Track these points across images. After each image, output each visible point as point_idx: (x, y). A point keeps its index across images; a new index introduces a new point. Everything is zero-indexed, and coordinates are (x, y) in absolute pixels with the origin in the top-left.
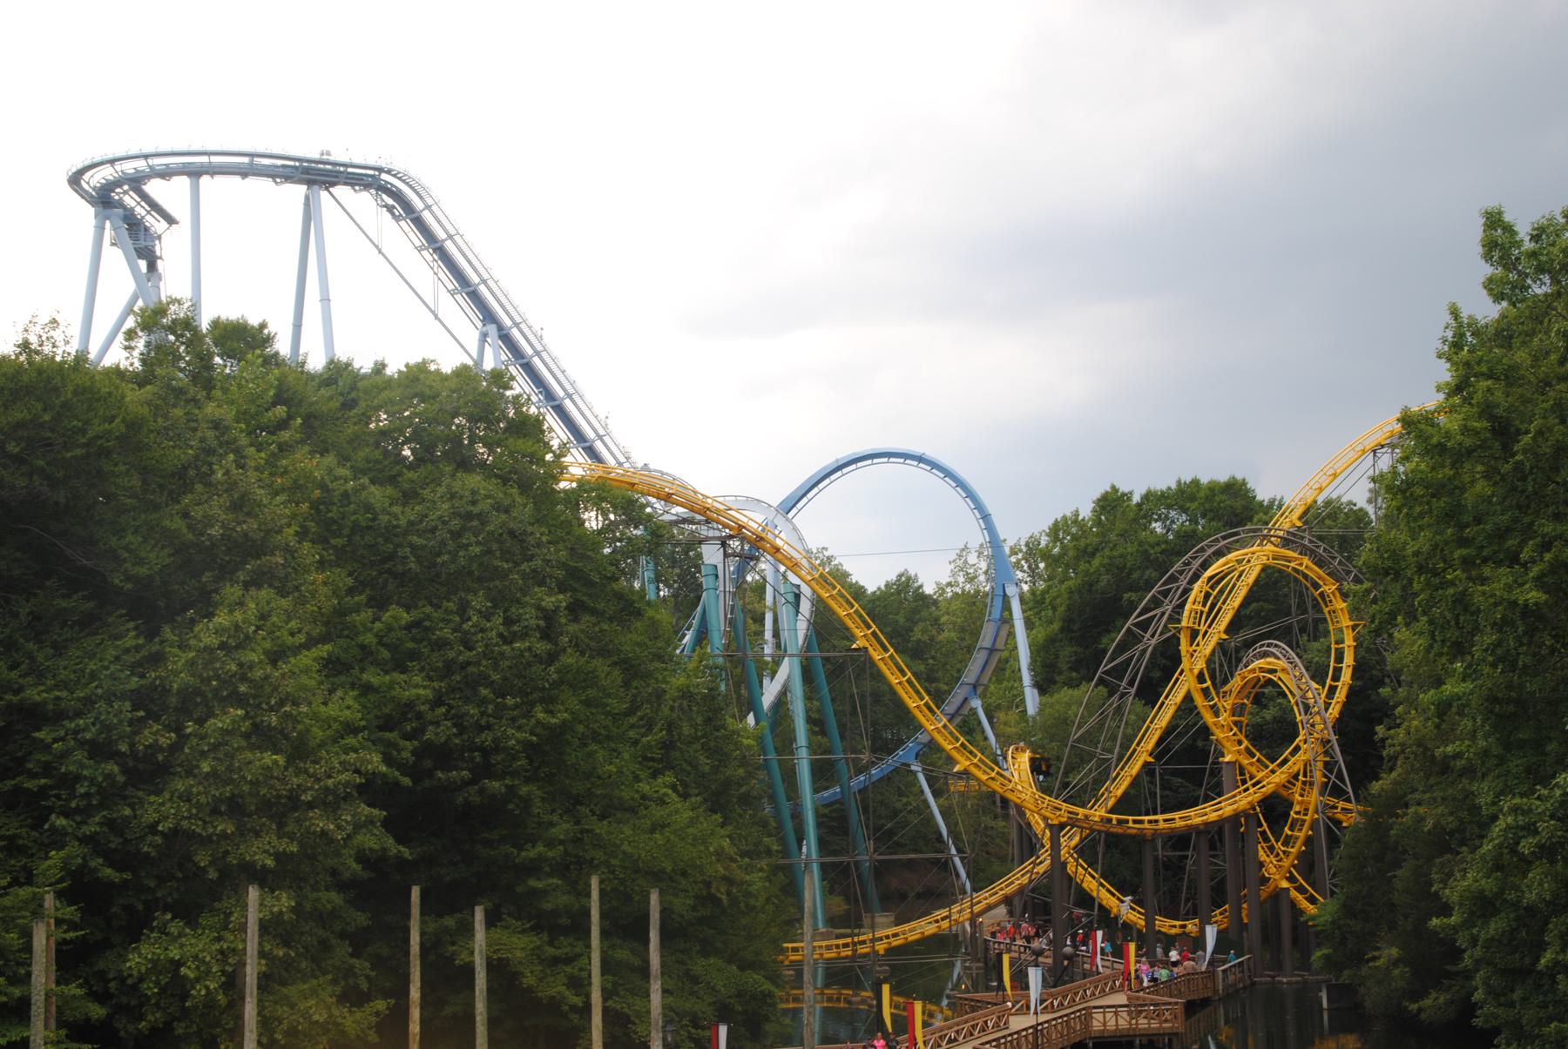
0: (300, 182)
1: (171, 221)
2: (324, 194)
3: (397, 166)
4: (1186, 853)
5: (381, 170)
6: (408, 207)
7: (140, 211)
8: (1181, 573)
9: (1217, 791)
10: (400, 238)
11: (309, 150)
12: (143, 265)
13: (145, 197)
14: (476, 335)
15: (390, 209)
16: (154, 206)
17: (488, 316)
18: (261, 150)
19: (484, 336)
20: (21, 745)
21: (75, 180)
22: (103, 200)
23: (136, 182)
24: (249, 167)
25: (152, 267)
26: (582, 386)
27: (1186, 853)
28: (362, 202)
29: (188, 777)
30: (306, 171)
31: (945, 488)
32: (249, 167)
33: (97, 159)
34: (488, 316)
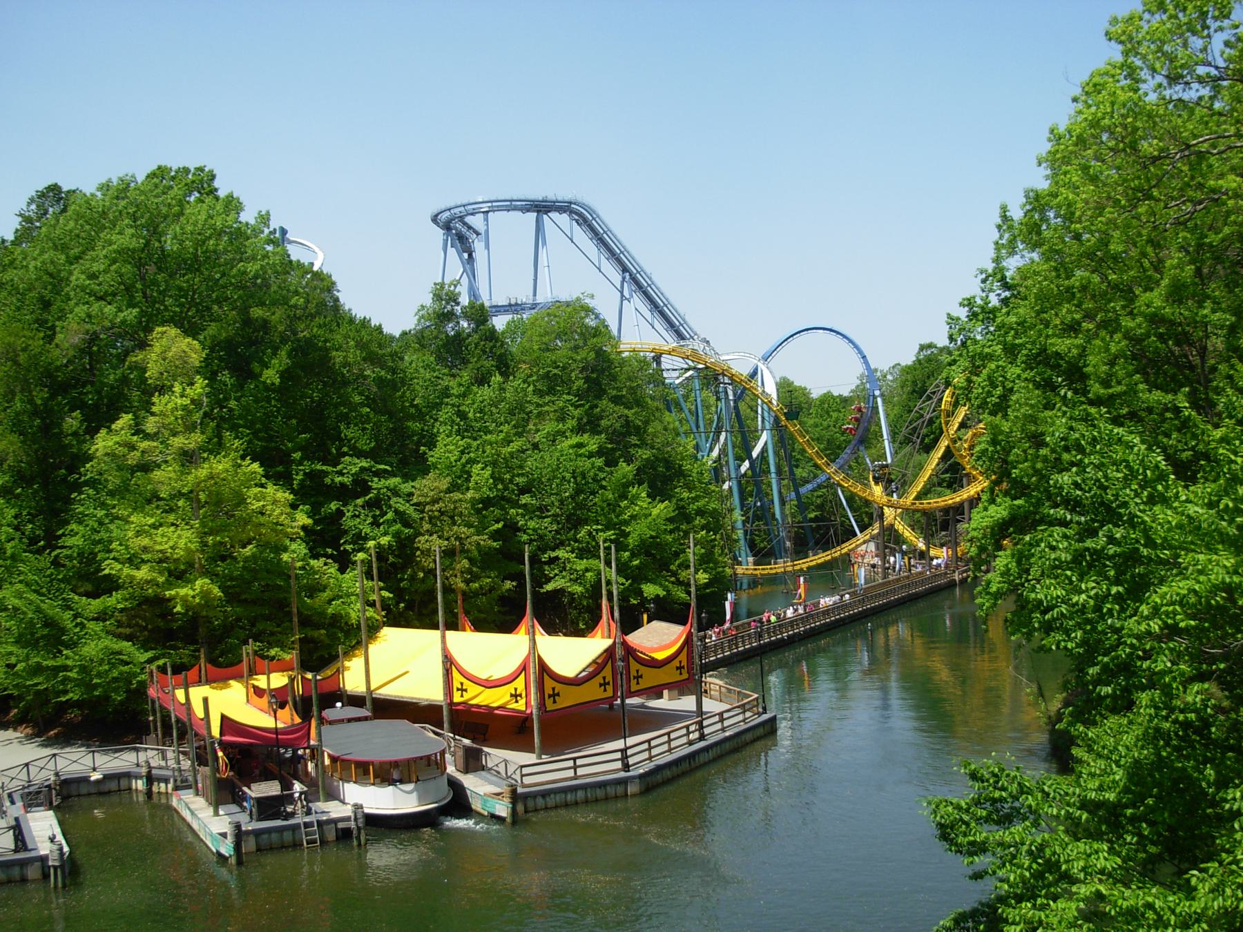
0: (534, 211)
1: (478, 234)
2: (545, 216)
3: (579, 199)
4: (446, 725)
5: (571, 203)
6: (585, 220)
7: (464, 230)
8: (934, 393)
9: (690, 605)
10: (581, 235)
11: (537, 194)
12: (466, 255)
13: (465, 224)
14: (620, 278)
15: (577, 221)
16: (470, 227)
17: (625, 270)
18: (515, 198)
19: (624, 278)
20: (562, 419)
21: (435, 219)
22: (447, 227)
23: (461, 219)
24: (511, 206)
25: (470, 255)
26: (672, 300)
27: (446, 725)
28: (563, 219)
29: (600, 447)
30: (536, 206)
31: (844, 343)
32: (511, 206)
33: (443, 209)
34: (625, 270)
